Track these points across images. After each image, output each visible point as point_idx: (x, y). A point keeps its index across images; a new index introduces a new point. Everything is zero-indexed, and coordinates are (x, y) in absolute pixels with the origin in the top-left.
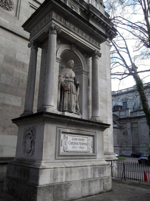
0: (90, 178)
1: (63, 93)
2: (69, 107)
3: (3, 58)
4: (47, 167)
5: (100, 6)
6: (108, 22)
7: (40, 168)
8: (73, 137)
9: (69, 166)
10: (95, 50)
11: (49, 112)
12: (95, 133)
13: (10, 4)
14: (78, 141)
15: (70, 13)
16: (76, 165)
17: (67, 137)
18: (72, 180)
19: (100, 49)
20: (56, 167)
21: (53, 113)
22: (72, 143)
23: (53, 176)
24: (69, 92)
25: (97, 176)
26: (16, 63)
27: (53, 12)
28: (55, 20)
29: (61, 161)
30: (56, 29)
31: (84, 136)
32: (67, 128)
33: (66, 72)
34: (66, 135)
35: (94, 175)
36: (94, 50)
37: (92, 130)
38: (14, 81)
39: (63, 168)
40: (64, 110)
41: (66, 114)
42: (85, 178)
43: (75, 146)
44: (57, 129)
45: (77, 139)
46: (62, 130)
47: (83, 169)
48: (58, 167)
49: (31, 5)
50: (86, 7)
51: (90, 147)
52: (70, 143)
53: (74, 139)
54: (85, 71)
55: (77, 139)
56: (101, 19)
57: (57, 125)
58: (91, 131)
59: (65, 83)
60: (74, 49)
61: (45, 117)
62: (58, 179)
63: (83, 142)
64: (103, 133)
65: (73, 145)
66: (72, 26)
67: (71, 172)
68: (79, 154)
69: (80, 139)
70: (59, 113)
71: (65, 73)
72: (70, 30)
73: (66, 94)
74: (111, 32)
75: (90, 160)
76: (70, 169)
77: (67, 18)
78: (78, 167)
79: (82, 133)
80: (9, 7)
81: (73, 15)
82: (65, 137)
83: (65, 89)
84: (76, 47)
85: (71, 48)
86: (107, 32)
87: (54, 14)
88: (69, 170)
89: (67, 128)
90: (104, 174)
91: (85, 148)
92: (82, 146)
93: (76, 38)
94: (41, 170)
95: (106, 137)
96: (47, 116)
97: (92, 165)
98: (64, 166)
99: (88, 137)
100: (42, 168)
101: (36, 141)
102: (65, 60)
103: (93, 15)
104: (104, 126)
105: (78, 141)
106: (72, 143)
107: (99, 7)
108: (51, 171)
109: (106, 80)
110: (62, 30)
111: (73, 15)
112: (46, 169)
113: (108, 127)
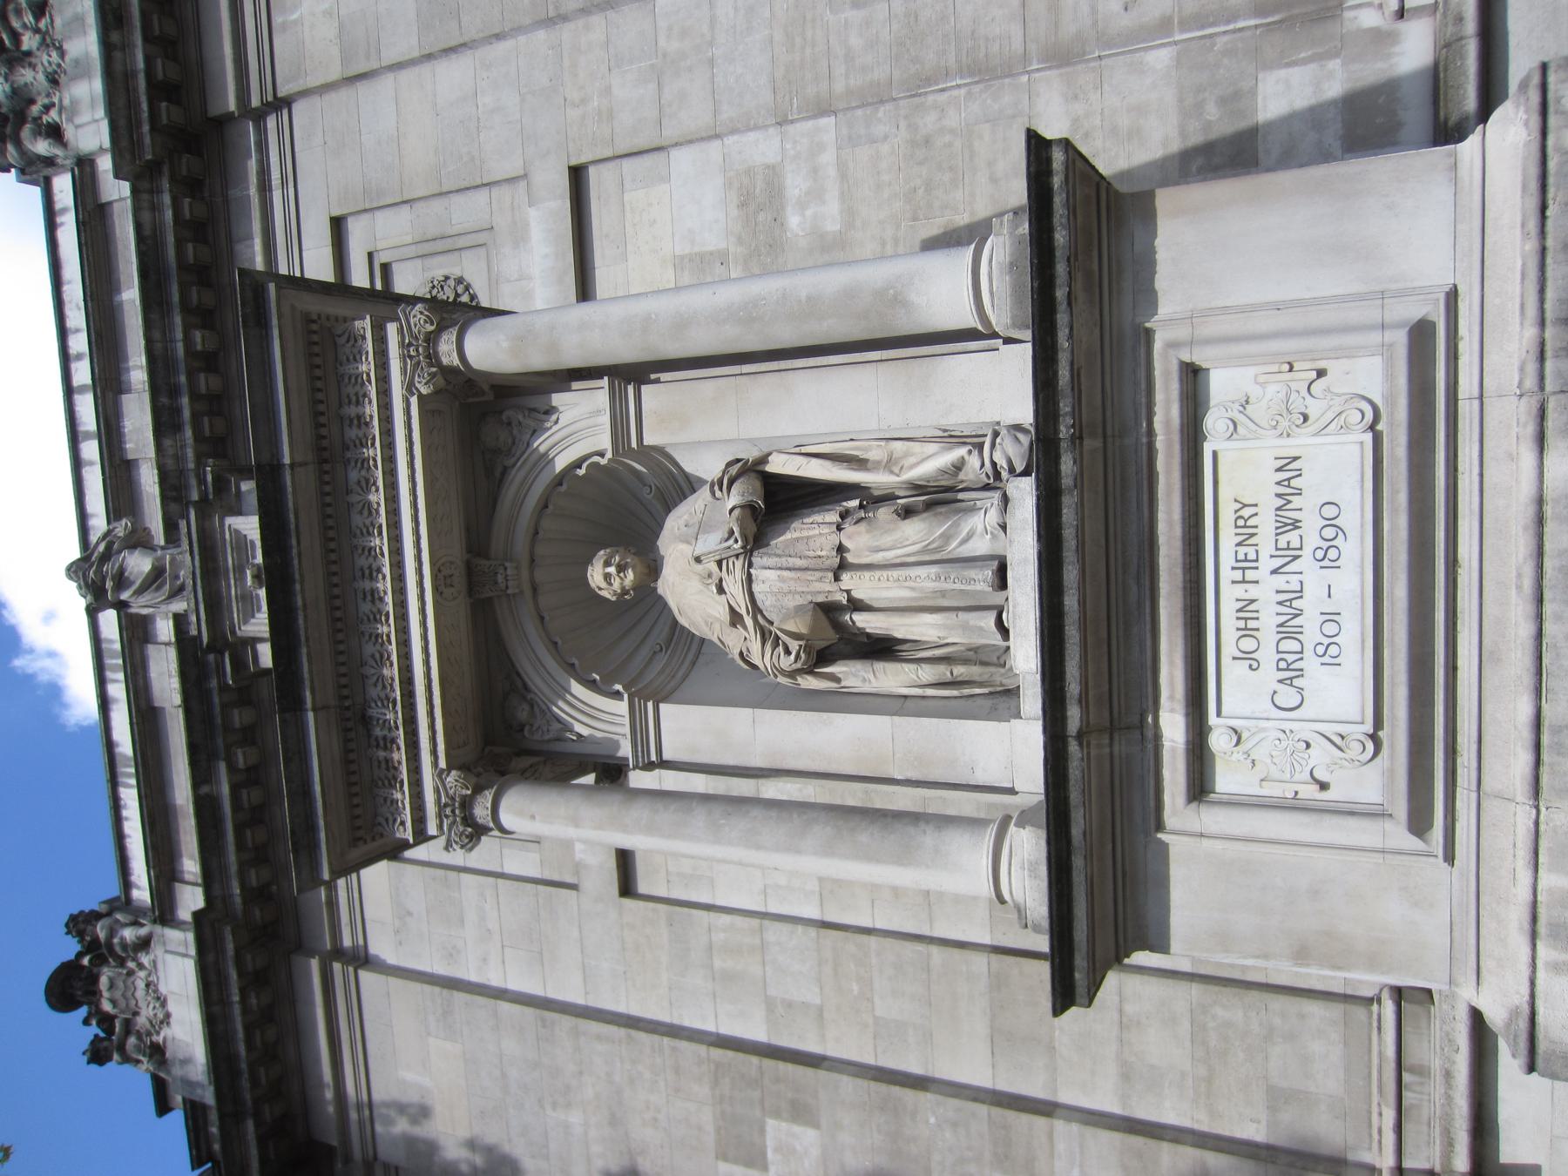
8: (1225, 660)
14: (1266, 591)
22: (1291, 673)
34: (1218, 741)
36: (414, 400)
48: (1523, 892)
52: (1288, 697)
53: (1248, 644)
63: (1266, 524)
65: (1310, 663)
70: (1032, 700)
82: (1238, 755)
91: (1337, 470)
99: (1208, 449)
106: (1291, 673)
110: (443, 764)
113: (1058, 157)
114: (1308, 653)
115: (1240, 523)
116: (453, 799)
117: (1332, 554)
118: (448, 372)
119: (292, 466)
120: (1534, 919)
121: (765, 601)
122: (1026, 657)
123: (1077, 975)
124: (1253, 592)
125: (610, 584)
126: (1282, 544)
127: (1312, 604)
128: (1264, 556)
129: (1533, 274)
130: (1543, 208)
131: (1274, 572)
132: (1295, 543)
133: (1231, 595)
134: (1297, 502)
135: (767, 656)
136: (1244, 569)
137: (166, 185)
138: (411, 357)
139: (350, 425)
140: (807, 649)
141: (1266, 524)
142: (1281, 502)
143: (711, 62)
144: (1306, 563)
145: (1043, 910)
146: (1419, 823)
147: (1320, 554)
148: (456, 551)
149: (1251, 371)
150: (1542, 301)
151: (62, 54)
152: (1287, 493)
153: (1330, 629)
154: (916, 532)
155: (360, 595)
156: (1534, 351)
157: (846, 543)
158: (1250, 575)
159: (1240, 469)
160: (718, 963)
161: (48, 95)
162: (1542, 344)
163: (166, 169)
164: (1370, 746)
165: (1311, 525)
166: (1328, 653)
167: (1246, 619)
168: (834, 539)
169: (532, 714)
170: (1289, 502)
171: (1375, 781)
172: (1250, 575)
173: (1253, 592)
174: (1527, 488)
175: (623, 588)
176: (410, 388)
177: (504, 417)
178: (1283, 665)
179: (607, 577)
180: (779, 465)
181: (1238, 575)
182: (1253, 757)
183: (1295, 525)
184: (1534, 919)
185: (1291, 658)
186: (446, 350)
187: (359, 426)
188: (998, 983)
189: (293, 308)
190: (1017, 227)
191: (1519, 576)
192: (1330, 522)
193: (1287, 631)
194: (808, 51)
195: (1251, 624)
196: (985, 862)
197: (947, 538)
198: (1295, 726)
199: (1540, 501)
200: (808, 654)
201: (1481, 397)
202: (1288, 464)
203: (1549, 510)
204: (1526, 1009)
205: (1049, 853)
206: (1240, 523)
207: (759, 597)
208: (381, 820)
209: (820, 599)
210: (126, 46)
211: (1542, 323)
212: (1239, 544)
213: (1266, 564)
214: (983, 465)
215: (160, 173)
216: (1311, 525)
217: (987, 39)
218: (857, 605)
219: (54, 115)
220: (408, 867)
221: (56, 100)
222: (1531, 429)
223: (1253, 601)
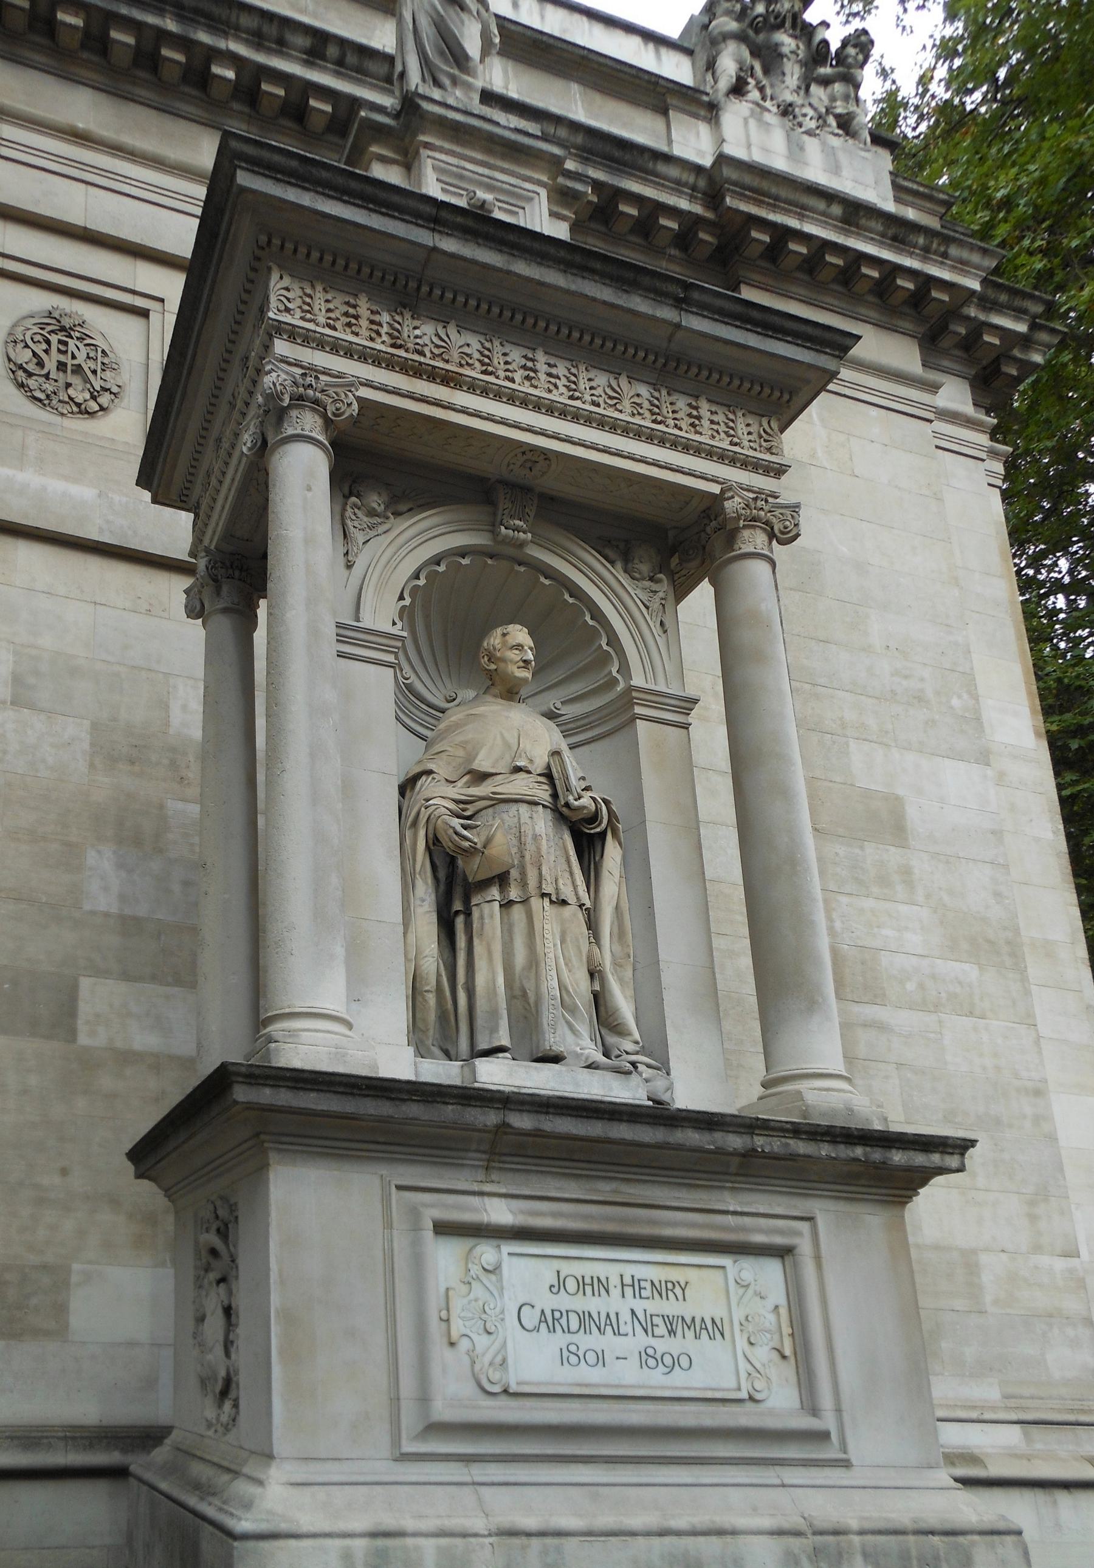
1: (458, 906)
2: (526, 1012)
3: (86, 746)
4: (306, 1522)
5: (836, 142)
6: (926, 250)
7: (245, 1525)
8: (556, 1264)
9: (530, 1523)
10: (728, 488)
11: (297, 1063)
12: (804, 1227)
13: (94, 372)
14: (616, 1303)
15: (424, 237)
16: (606, 1520)
17: (494, 1271)
20: (389, 1521)
21: (341, 1069)
24: (514, 894)
26: (173, 764)
27: (275, 276)
28: (293, 334)
30: (316, 402)
33: (469, 733)
34: (487, 1252)
36: (716, 489)
37: (761, 1203)
38: (176, 888)
39: (464, 1535)
40: (483, 1045)
41: (493, 1074)
43: (590, 1341)
44: (386, 1201)
45: (601, 1286)
46: (436, 1208)
48: (409, 1524)
50: (692, 198)
51: (763, 1354)
52: (530, 1318)
53: (571, 1285)
54: (656, 699)
55: (601, 1286)
56: (772, 217)
57: (384, 1170)
58: (758, 1211)
59: (456, 822)
60: (517, 529)
61: (250, 1106)
63: (671, 1307)
65: (560, 1339)
66: (465, 343)
69: (637, 1286)
70: (439, 1071)
71: (463, 745)
72: (448, 380)
73: (488, 910)
74: (979, 328)
75: (770, 1475)
76: (545, 1552)
77: (410, 287)
78: (633, 1534)
79: (668, 1232)
80: (88, 396)
81: (449, 245)
82: (475, 1270)
83: (473, 869)
84: (532, 511)
85: (494, 533)
86: (946, 342)
87: (287, 281)
89: (488, 1188)
91: (712, 1368)
92: (664, 1345)
94: (251, 1544)
95: (1060, 1264)
96: (266, 1095)
97: (794, 1521)
98: (479, 1524)
100: (263, 1527)
101: (242, 1303)
102: (448, 635)
103: (767, 239)
104: (898, 1157)
105: (616, 1303)
106: (551, 1321)
107: (830, 153)
108: (347, 1556)
109: (984, 757)
110: (364, 392)
111: (449, 245)
113: (953, 1161)
114: (569, 1338)
115: (670, 1286)
117: (652, 1362)
123: (267, 1091)
124: (616, 1292)
125: (512, 648)
126: (656, 1320)
127: (607, 1342)
128: (645, 1304)
130: (880, 1532)
131: (633, 1312)
132: (657, 1331)
134: (690, 1334)
136: (633, 1286)
137: (698, 209)
138: (755, 499)
139: (690, 405)
140: (472, 851)
141: (671, 1307)
142: (688, 1320)
144: (642, 1340)
147: (650, 1351)
148: (550, 482)
149: (782, 1301)
150: (694, 1533)
151: (810, 133)
152: (697, 1326)
153: (591, 1357)
157: (567, 911)
158: (629, 1291)
159: (708, 1286)
161: (772, 99)
163: (709, 215)
164: (496, 1389)
166: (566, 1356)
167: (592, 1285)
168: (572, 899)
169: (372, 513)
170: (689, 1328)
172: (629, 1291)
174: (742, 1522)
175: (503, 660)
177: (661, 576)
178: (557, 1315)
179: (519, 647)
181: (628, 1280)
182: (474, 1283)
183: (672, 1332)
185: (564, 1321)
186: (309, 422)
187: (690, 415)
189: (808, 382)
190: (878, 1119)
192: (676, 1362)
193: (586, 1319)
195: (588, 1289)
197: (572, 1010)
199: (734, 1533)
201: (783, 1486)
202: (715, 1329)
203: (728, 1539)
205: (399, 1081)
206: (670, 1286)
207: (514, 808)
209: (514, 874)
210: (824, 218)
212: (652, 1283)
213: (639, 1306)
214: (627, 1053)
215: (707, 207)
217: (737, 1078)
219: (755, 95)
221: (768, 104)
222: (786, 1525)
223: (608, 1292)
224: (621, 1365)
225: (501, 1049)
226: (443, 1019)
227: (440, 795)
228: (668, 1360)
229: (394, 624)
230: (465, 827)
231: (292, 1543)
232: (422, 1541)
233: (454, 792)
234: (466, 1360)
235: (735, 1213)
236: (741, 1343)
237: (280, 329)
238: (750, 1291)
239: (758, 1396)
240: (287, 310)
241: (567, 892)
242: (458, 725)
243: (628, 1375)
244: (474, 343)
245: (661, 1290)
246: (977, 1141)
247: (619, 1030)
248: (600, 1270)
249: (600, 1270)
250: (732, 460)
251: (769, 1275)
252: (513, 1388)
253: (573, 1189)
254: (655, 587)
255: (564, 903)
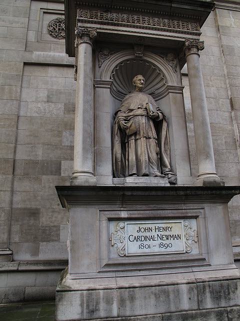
0: (187, 309)
3: (63, 109)
8: (139, 226)
18: (137, 313)
19: (199, 34)
23: (88, 306)
25: (209, 304)
29: (113, 274)
31: (171, 222)
32: (122, 209)
33: (129, 101)
34: (121, 224)
35: (199, 302)
36: (184, 40)
37: (191, 206)
42: (173, 309)
43: (148, 242)
45: (150, 230)
47: (163, 292)
48: (98, 287)
49: (46, 11)
52: (132, 238)
53: (142, 230)
58: (191, 208)
60: (139, 53)
62: (99, 310)
63: (167, 233)
64: (227, 208)
65: (139, 243)
67: (132, 298)
68: (156, 260)
69: (159, 229)
72: (118, 25)
75: (190, 270)
76: (130, 291)
88: (127, 293)
90: (229, 299)
91: (178, 246)
93: (166, 36)
99: (182, 221)
106: (137, 239)
108: (82, 295)
110: (98, 30)
112: (71, 291)
116: (89, 32)
117: (162, 246)
118: (189, 49)
119: (171, 6)
120: (92, 290)
121: (137, 119)
122: (130, 181)
124: (154, 231)
127: (151, 242)
129: (217, 279)
133: (153, 226)
135: (122, 118)
140: (127, 128)
143: (217, 110)
144: (160, 241)
145: (77, 184)
146: (107, 265)
147: (162, 244)
149: (196, 229)
150: (212, 281)
153: (147, 246)
154: (154, 156)
155: (139, 16)
156: (204, 281)
157: (151, 140)
159: (177, 228)
160: (6, 87)
162: (205, 282)
165: (168, 242)
171: (115, 258)
173: (154, 231)
176: (188, 39)
179: (140, 80)
180: (165, 125)
181: (157, 228)
183: (167, 239)
184: (92, 290)
185: (140, 239)
188: (6, 161)
191: (163, 282)
193: (146, 238)
194: (218, 131)
196: (86, 170)
197: (152, 163)
198: (126, 240)
199: (177, 284)
200: (126, 128)
202: (179, 237)
203: (176, 286)
204: (71, 289)
207: (138, 117)
208: (81, 10)
211: (209, 282)
213: (159, 233)
216: (168, 242)
218: (136, 140)
220: (29, 3)
224: (155, 247)
225: (134, 174)
226: (119, 170)
227: (121, 115)
228: (166, 245)
229: (111, 78)
230: (125, 123)
231: (70, 292)
232: (100, 291)
233: (125, 115)
234: (116, 249)
235: (192, 209)
236: (184, 240)
237: (79, 21)
238: (188, 227)
239: (188, 252)
240: (81, 16)
241: (150, 135)
242: (127, 99)
243: (156, 250)
244: (125, 16)
245: (165, 229)
246: (56, 187)
247: (166, 167)
248: (150, 226)
249: (150, 226)
250: (188, 33)
251: (194, 222)
252: (127, 255)
253: (144, 207)
254: (174, 62)
255: (150, 138)
